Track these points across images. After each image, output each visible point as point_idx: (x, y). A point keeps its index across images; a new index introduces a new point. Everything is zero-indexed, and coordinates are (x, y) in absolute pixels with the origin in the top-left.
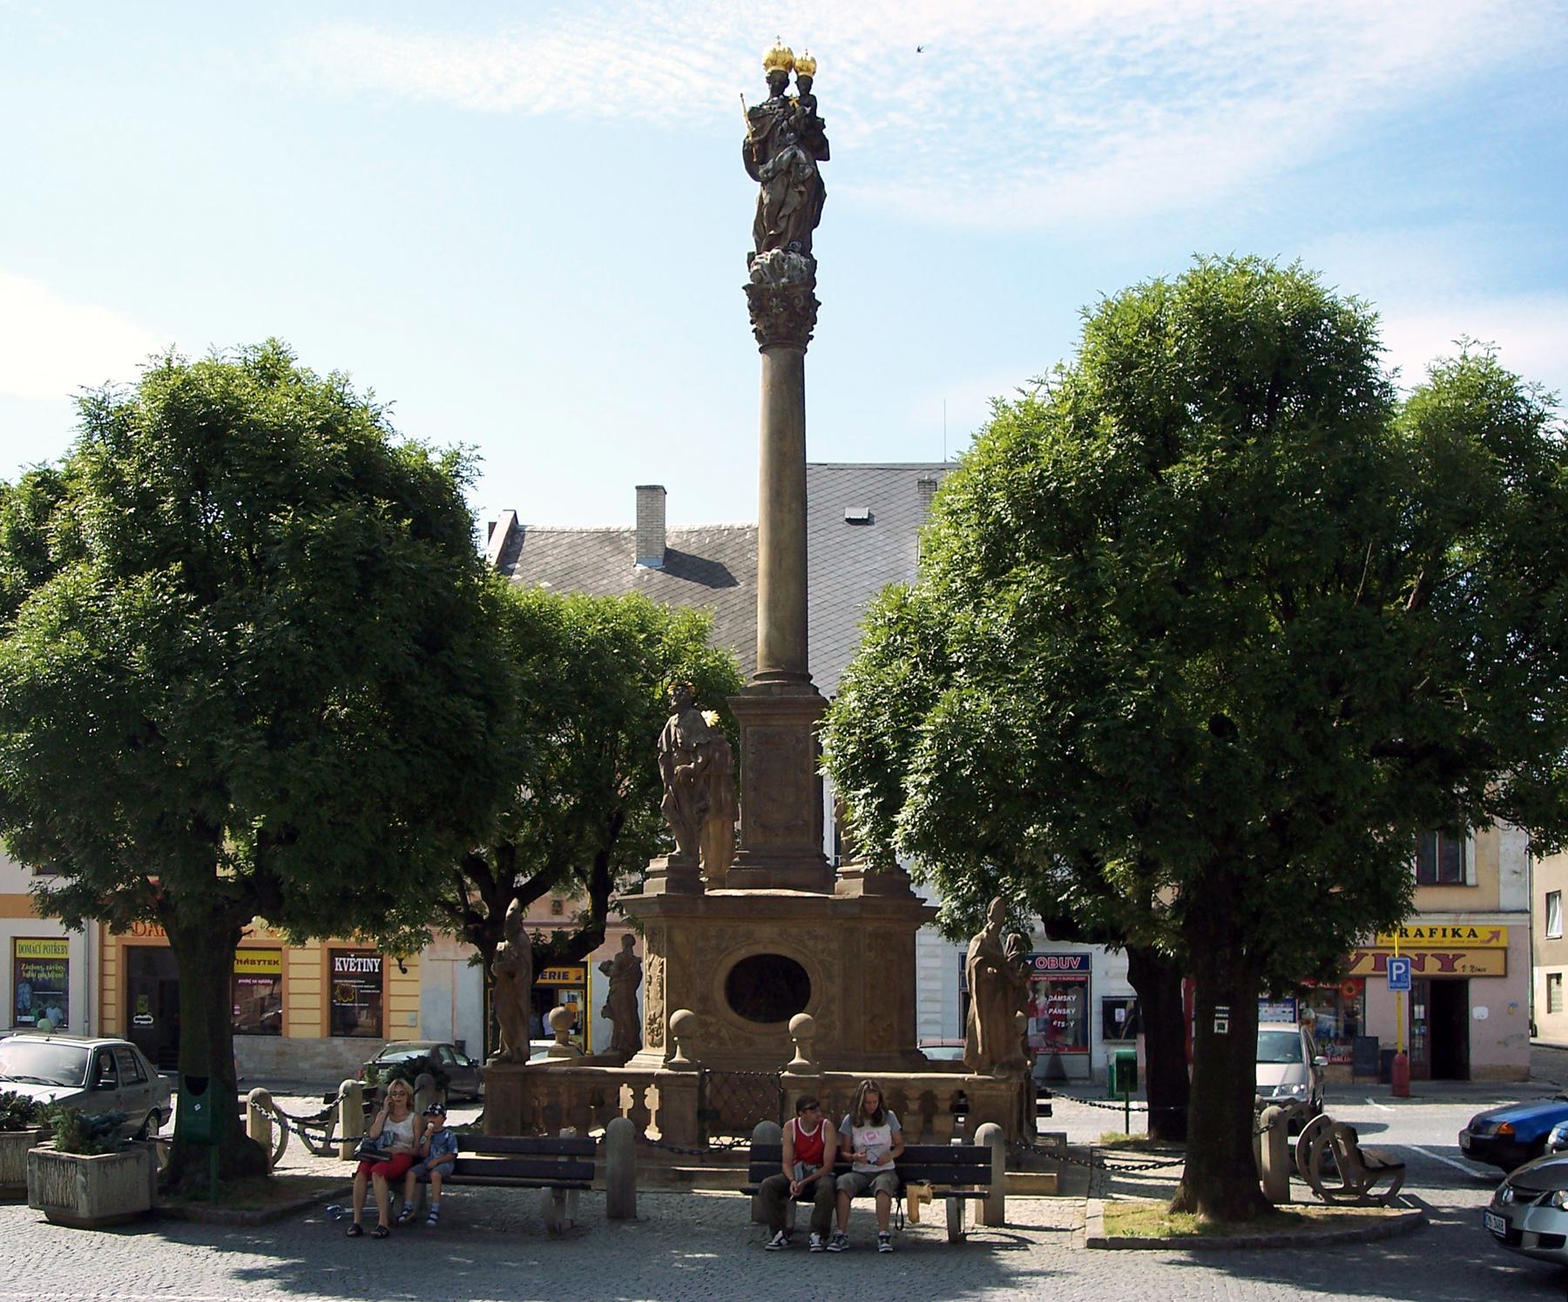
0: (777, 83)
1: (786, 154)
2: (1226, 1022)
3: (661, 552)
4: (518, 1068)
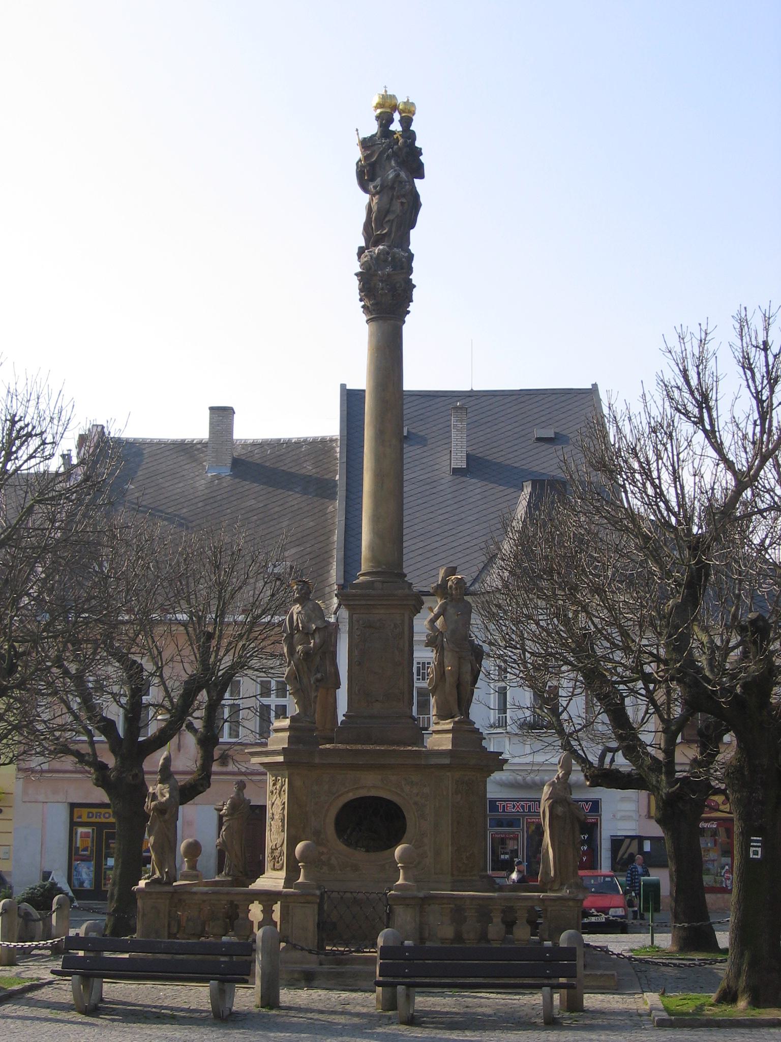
0: (385, 120)
1: (391, 175)
2: (759, 850)
3: (229, 461)
4: (167, 888)
